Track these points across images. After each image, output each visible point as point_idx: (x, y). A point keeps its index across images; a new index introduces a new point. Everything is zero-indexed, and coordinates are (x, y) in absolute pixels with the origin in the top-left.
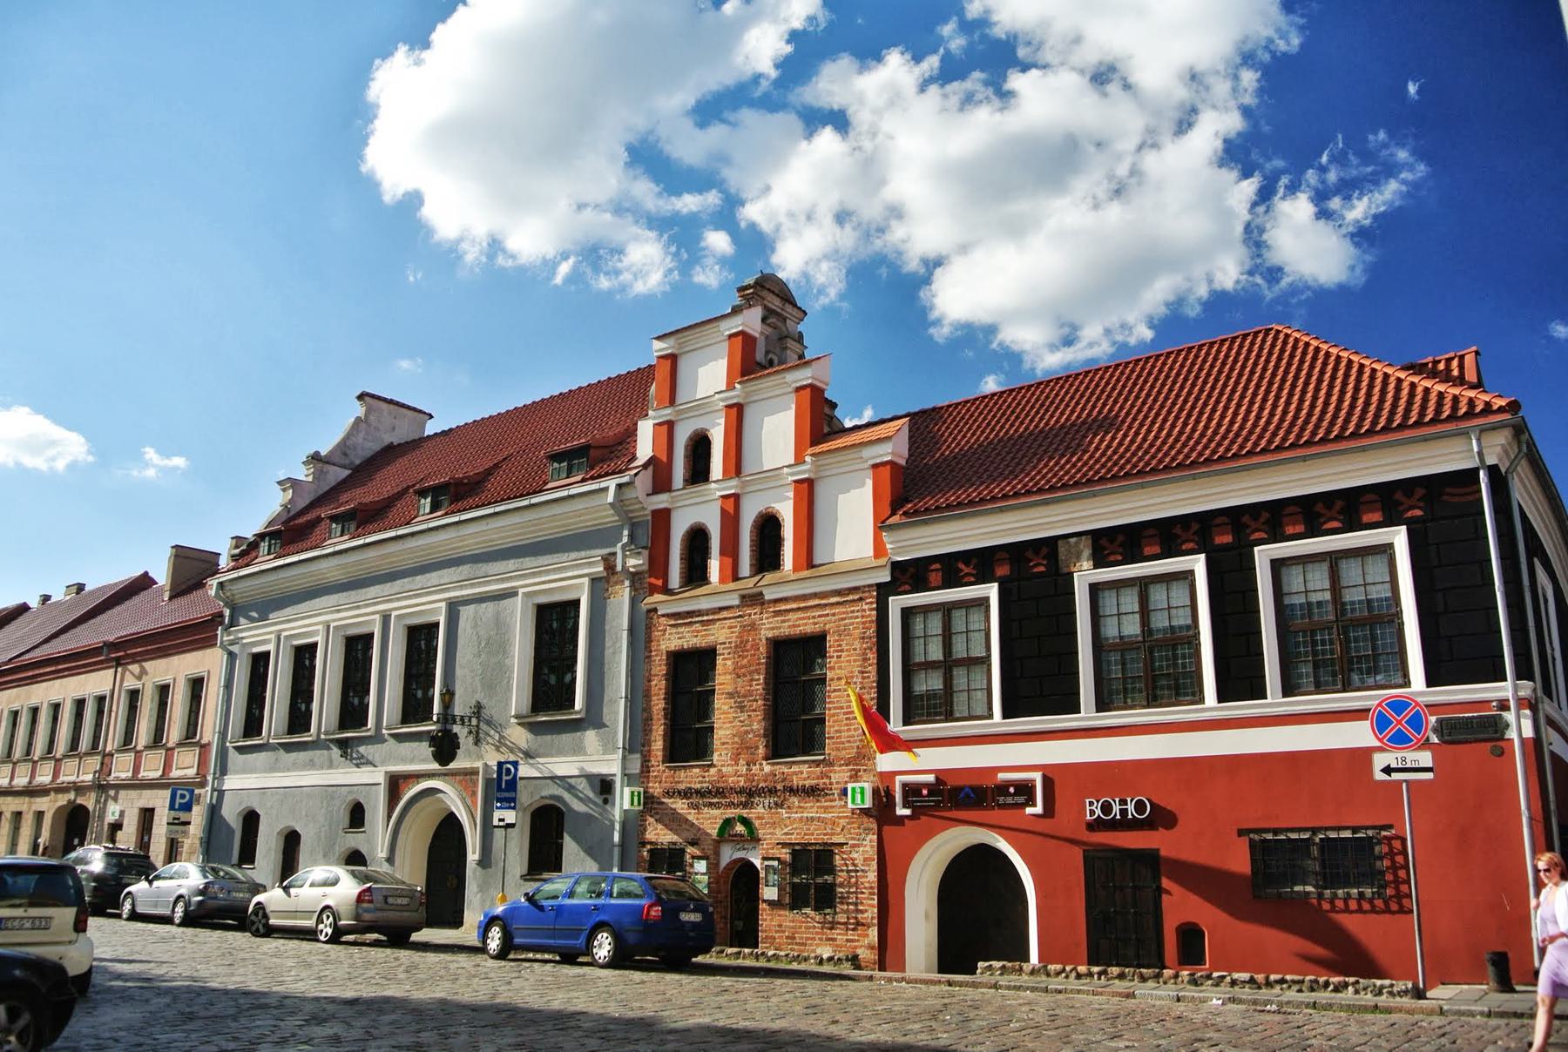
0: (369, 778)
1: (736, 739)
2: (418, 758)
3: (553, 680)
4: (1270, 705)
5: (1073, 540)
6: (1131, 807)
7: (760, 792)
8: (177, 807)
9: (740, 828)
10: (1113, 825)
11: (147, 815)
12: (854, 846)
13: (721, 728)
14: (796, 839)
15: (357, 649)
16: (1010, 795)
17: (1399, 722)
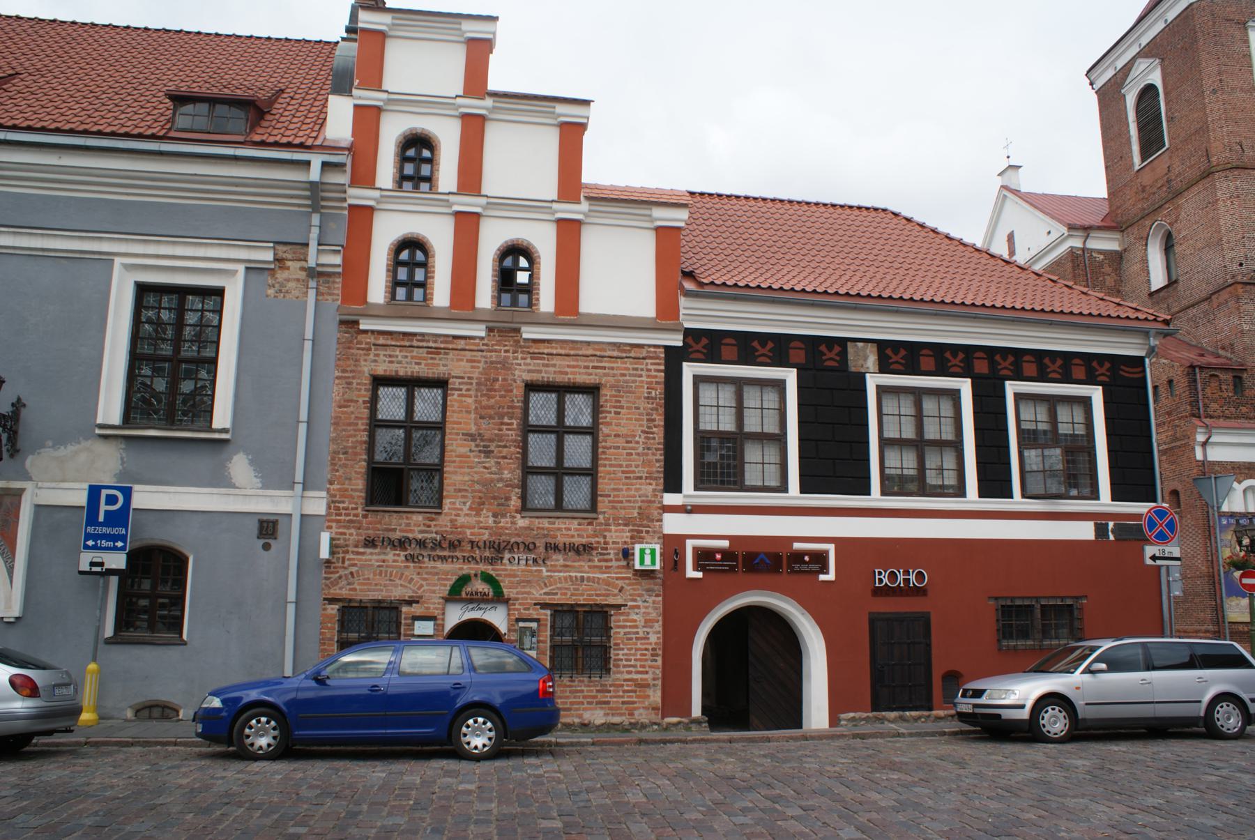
1: (477, 487)
3: (160, 385)
4: (967, 502)
5: (860, 344)
6: (912, 577)
7: (512, 547)
8: (101, 519)
9: (479, 586)
10: (897, 592)
12: (633, 607)
13: (455, 473)
14: (559, 599)
16: (805, 563)
17: (1161, 525)
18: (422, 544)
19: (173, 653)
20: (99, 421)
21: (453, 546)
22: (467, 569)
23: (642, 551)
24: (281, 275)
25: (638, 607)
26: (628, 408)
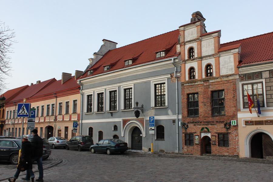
0: (118, 120)
1: (204, 112)
2: (131, 117)
9: (205, 130)
11: (66, 128)
15: (100, 95)
18: (196, 122)
19: (163, 142)
20: (151, 107)
21: (201, 123)
22: (203, 126)
23: (233, 122)
24: (173, 79)
25: (233, 133)
26: (230, 93)
